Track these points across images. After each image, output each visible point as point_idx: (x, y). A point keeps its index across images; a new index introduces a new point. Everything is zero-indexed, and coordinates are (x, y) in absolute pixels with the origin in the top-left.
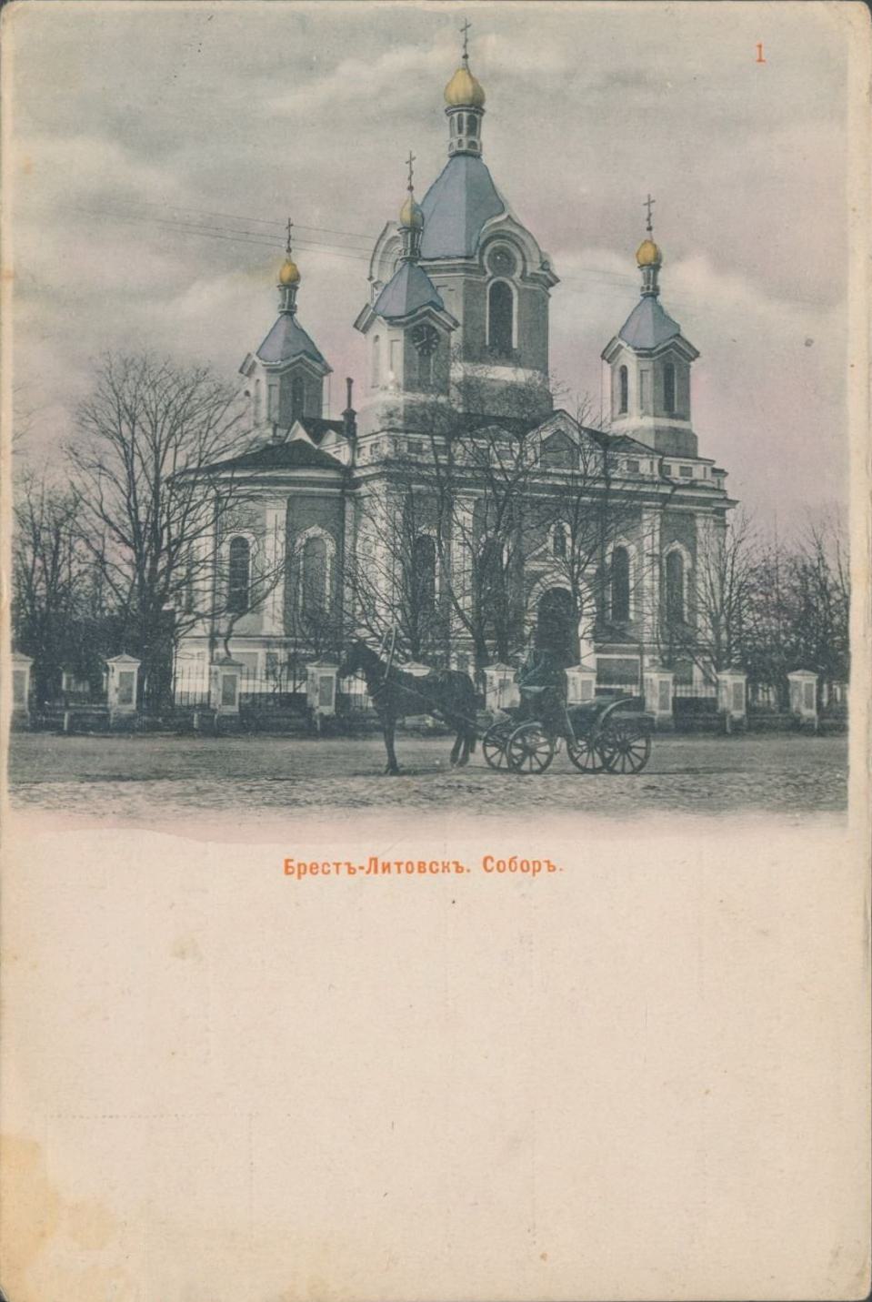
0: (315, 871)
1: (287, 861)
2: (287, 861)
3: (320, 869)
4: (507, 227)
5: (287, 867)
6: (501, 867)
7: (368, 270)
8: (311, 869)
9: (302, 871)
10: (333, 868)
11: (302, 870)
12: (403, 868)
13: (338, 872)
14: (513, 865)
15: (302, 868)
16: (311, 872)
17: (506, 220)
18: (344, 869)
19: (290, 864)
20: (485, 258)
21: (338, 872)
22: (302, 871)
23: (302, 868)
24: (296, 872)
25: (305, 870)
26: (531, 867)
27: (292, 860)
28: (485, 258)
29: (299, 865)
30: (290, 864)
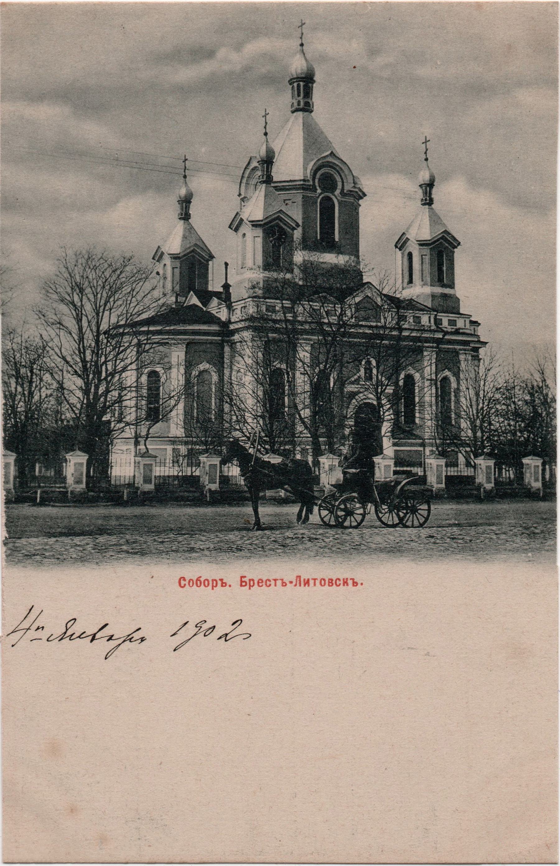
0: (260, 584)
1: (242, 577)
2: (242, 577)
5: (242, 582)
8: (258, 583)
10: (273, 583)
12: (318, 582)
13: (275, 585)
18: (279, 583)
19: (243, 579)
22: (215, 585)
27: (245, 577)
30: (243, 579)
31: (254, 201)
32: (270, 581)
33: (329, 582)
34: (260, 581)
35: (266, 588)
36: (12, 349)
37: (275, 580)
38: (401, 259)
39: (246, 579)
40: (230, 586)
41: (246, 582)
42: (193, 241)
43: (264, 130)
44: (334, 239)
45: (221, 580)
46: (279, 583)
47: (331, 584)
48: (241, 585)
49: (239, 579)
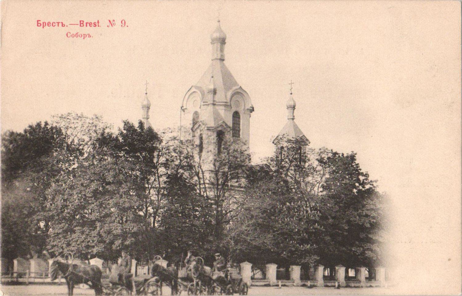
0: (49, 25)
1: (38, 21)
2: (38, 21)
3: (51, 24)
4: (239, 91)
5: (38, 23)
6: (73, 36)
7: (272, 288)
8: (48, 24)
9: (44, 25)
10: (57, 24)
11: (44, 25)
12: (88, 25)
13: (58, 26)
14: (77, 35)
15: (44, 24)
16: (48, 26)
17: (239, 88)
18: (60, 24)
19: (39, 22)
20: (201, 258)
21: (58, 26)
22: (44, 25)
23: (44, 24)
24: (42, 26)
25: (46, 25)
26: (84, 36)
27: (40, 21)
28: (201, 258)
29: (43, 23)
30: (39, 22)
31: (221, 108)
32: (55, 23)
33: (83, 24)
34: (49, 23)
35: (53, 27)
36: (202, 247)
37: (58, 23)
38: (260, 285)
39: (41, 22)
40: (127, 26)
41: (41, 24)
42: (220, 122)
43: (210, 105)
44: (216, 253)
45: (62, 23)
46: (60, 24)
47: (82, 25)
48: (38, 26)
49: (36, 22)
